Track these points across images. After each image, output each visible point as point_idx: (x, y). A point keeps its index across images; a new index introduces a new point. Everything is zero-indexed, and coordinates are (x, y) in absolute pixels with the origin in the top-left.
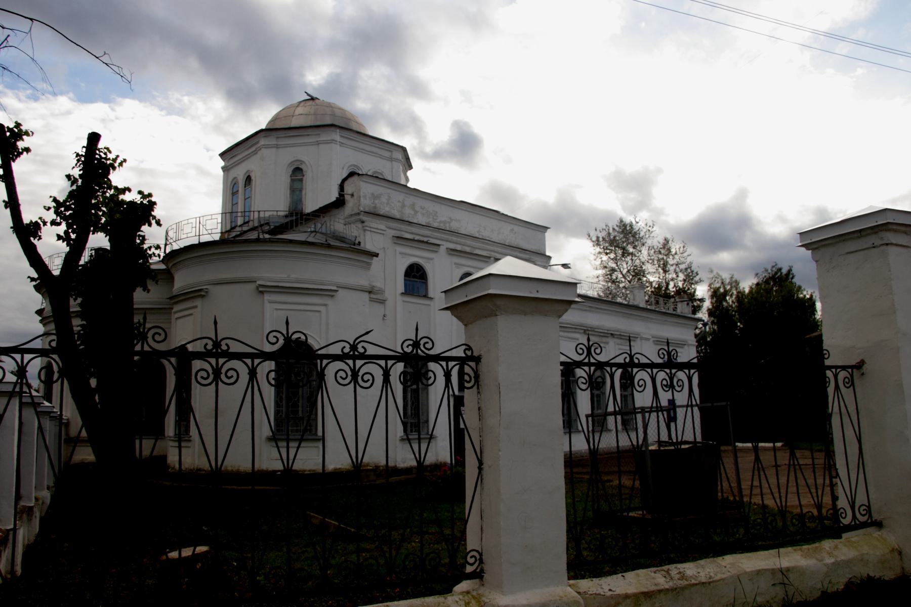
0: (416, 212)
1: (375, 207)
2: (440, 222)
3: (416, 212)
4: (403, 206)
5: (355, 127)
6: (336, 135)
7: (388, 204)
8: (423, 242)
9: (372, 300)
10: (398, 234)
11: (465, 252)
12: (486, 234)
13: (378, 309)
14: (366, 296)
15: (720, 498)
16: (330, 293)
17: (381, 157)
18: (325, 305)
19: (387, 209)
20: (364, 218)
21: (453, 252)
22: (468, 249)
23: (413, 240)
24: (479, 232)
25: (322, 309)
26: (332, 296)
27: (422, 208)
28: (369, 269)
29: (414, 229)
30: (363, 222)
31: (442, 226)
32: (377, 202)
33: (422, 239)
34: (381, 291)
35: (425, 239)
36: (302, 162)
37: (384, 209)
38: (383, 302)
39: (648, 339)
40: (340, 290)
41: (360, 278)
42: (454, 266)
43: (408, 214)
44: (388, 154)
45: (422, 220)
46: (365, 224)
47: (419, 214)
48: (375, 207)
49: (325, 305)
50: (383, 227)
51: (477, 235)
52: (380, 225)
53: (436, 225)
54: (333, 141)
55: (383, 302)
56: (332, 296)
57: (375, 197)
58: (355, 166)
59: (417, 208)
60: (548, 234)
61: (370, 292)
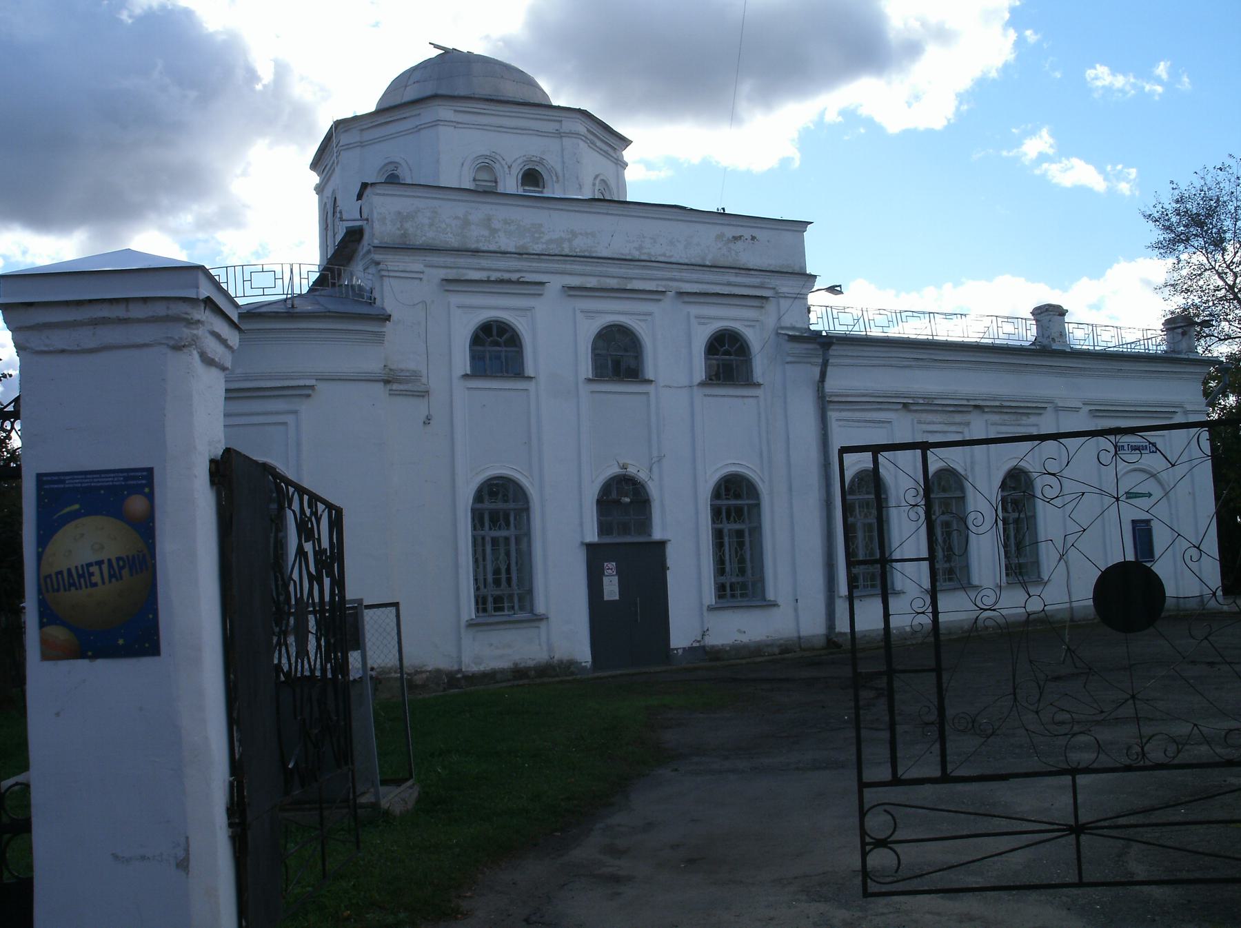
0: (494, 231)
1: (404, 235)
2: (551, 241)
3: (494, 231)
4: (466, 223)
5: (510, 90)
6: (444, 112)
7: (431, 225)
8: (509, 282)
9: (392, 393)
10: (452, 274)
11: (586, 289)
12: (658, 250)
13: (419, 408)
14: (379, 387)
15: (276, 661)
16: (305, 392)
17: (539, 133)
18: (295, 412)
19: (431, 234)
20: (377, 257)
21: (571, 291)
22: (613, 283)
23: (488, 281)
24: (640, 248)
25: (290, 419)
26: (309, 396)
27: (506, 222)
28: (382, 342)
29: (484, 263)
30: (378, 263)
31: (553, 249)
32: (408, 225)
33: (506, 276)
34: (415, 376)
35: (514, 277)
36: (396, 165)
37: (428, 236)
38: (424, 394)
39: (1076, 410)
40: (320, 386)
41: (369, 360)
42: (579, 316)
43: (475, 236)
44: (551, 127)
45: (506, 243)
46: (381, 266)
47: (501, 234)
48: (404, 235)
49: (295, 412)
50: (418, 266)
51: (636, 255)
52: (414, 263)
53: (538, 248)
54: (436, 123)
55: (424, 394)
56: (309, 396)
57: (402, 217)
58: (486, 157)
59: (496, 224)
60: (809, 235)
61: (387, 382)
